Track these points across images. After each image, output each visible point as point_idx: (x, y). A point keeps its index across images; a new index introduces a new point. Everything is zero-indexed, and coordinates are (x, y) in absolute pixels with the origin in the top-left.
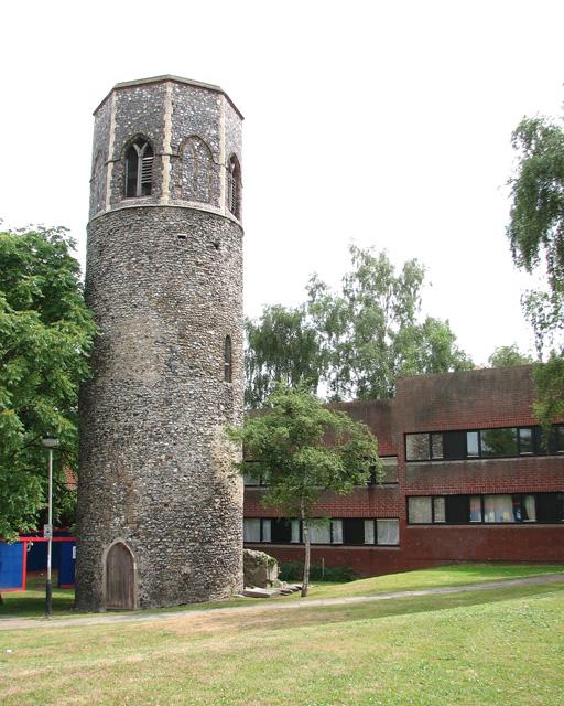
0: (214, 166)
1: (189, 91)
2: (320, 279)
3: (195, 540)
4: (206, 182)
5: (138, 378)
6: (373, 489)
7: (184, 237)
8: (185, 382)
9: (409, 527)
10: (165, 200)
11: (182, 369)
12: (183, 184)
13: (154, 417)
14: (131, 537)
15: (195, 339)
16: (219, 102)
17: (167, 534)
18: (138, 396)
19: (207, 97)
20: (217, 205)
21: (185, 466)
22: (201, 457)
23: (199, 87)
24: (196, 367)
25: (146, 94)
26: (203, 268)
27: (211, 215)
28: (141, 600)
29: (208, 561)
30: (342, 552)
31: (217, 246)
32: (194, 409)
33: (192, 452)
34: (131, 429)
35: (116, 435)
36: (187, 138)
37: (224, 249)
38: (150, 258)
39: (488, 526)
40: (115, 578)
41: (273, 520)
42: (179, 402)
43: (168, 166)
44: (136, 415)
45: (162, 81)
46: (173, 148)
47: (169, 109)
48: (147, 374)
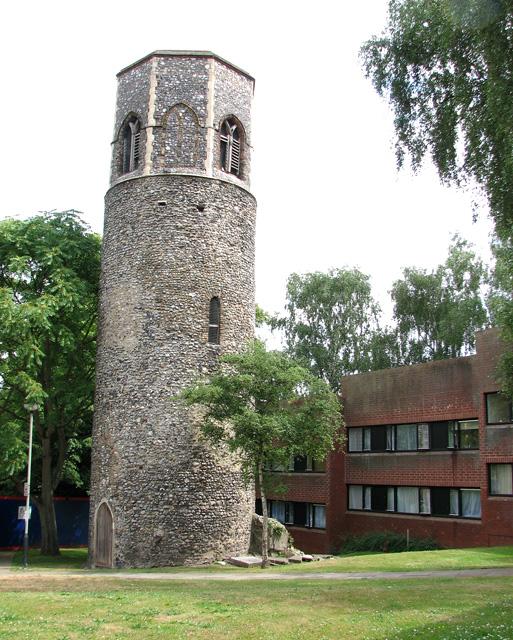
0: (201, 131)
1: (175, 62)
2: (463, 237)
3: (170, 503)
4: (190, 147)
5: (121, 344)
6: (456, 455)
7: (163, 204)
8: (162, 345)
9: (491, 498)
10: (148, 171)
11: (159, 332)
12: (166, 152)
13: (133, 381)
14: (112, 497)
15: (173, 303)
16: (207, 67)
17: (141, 496)
18: (121, 362)
19: (192, 65)
20: (203, 168)
21: (159, 429)
22: (176, 420)
23: (185, 56)
24: (174, 330)
25: (137, 72)
26: (183, 231)
27: (193, 179)
28: (117, 559)
29: (183, 524)
30: (430, 525)
31: (201, 209)
32: (170, 372)
33: (167, 415)
34: (114, 394)
35: (105, 400)
36: (171, 108)
37: (210, 211)
38: (133, 228)
39: (498, 498)
40: (102, 537)
41: (433, 489)
42: (154, 365)
43: (151, 137)
44: (119, 379)
45: (148, 58)
46: (157, 119)
47: (154, 83)
48: (126, 340)
